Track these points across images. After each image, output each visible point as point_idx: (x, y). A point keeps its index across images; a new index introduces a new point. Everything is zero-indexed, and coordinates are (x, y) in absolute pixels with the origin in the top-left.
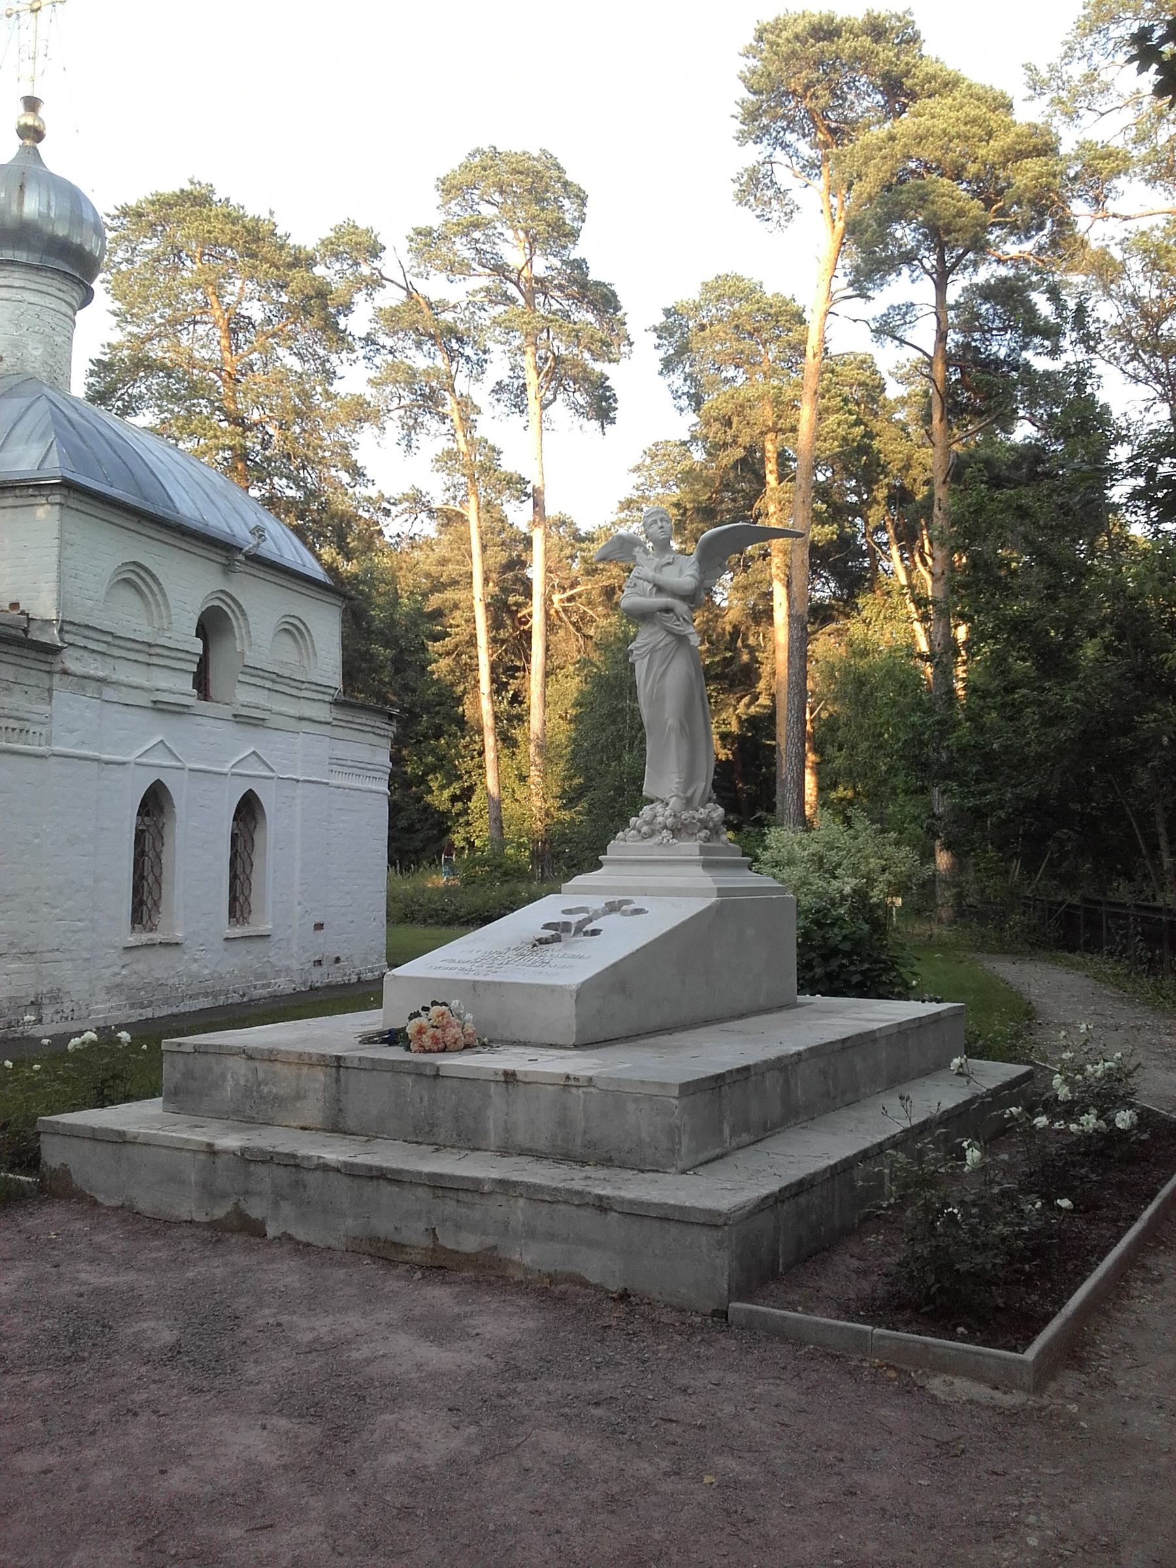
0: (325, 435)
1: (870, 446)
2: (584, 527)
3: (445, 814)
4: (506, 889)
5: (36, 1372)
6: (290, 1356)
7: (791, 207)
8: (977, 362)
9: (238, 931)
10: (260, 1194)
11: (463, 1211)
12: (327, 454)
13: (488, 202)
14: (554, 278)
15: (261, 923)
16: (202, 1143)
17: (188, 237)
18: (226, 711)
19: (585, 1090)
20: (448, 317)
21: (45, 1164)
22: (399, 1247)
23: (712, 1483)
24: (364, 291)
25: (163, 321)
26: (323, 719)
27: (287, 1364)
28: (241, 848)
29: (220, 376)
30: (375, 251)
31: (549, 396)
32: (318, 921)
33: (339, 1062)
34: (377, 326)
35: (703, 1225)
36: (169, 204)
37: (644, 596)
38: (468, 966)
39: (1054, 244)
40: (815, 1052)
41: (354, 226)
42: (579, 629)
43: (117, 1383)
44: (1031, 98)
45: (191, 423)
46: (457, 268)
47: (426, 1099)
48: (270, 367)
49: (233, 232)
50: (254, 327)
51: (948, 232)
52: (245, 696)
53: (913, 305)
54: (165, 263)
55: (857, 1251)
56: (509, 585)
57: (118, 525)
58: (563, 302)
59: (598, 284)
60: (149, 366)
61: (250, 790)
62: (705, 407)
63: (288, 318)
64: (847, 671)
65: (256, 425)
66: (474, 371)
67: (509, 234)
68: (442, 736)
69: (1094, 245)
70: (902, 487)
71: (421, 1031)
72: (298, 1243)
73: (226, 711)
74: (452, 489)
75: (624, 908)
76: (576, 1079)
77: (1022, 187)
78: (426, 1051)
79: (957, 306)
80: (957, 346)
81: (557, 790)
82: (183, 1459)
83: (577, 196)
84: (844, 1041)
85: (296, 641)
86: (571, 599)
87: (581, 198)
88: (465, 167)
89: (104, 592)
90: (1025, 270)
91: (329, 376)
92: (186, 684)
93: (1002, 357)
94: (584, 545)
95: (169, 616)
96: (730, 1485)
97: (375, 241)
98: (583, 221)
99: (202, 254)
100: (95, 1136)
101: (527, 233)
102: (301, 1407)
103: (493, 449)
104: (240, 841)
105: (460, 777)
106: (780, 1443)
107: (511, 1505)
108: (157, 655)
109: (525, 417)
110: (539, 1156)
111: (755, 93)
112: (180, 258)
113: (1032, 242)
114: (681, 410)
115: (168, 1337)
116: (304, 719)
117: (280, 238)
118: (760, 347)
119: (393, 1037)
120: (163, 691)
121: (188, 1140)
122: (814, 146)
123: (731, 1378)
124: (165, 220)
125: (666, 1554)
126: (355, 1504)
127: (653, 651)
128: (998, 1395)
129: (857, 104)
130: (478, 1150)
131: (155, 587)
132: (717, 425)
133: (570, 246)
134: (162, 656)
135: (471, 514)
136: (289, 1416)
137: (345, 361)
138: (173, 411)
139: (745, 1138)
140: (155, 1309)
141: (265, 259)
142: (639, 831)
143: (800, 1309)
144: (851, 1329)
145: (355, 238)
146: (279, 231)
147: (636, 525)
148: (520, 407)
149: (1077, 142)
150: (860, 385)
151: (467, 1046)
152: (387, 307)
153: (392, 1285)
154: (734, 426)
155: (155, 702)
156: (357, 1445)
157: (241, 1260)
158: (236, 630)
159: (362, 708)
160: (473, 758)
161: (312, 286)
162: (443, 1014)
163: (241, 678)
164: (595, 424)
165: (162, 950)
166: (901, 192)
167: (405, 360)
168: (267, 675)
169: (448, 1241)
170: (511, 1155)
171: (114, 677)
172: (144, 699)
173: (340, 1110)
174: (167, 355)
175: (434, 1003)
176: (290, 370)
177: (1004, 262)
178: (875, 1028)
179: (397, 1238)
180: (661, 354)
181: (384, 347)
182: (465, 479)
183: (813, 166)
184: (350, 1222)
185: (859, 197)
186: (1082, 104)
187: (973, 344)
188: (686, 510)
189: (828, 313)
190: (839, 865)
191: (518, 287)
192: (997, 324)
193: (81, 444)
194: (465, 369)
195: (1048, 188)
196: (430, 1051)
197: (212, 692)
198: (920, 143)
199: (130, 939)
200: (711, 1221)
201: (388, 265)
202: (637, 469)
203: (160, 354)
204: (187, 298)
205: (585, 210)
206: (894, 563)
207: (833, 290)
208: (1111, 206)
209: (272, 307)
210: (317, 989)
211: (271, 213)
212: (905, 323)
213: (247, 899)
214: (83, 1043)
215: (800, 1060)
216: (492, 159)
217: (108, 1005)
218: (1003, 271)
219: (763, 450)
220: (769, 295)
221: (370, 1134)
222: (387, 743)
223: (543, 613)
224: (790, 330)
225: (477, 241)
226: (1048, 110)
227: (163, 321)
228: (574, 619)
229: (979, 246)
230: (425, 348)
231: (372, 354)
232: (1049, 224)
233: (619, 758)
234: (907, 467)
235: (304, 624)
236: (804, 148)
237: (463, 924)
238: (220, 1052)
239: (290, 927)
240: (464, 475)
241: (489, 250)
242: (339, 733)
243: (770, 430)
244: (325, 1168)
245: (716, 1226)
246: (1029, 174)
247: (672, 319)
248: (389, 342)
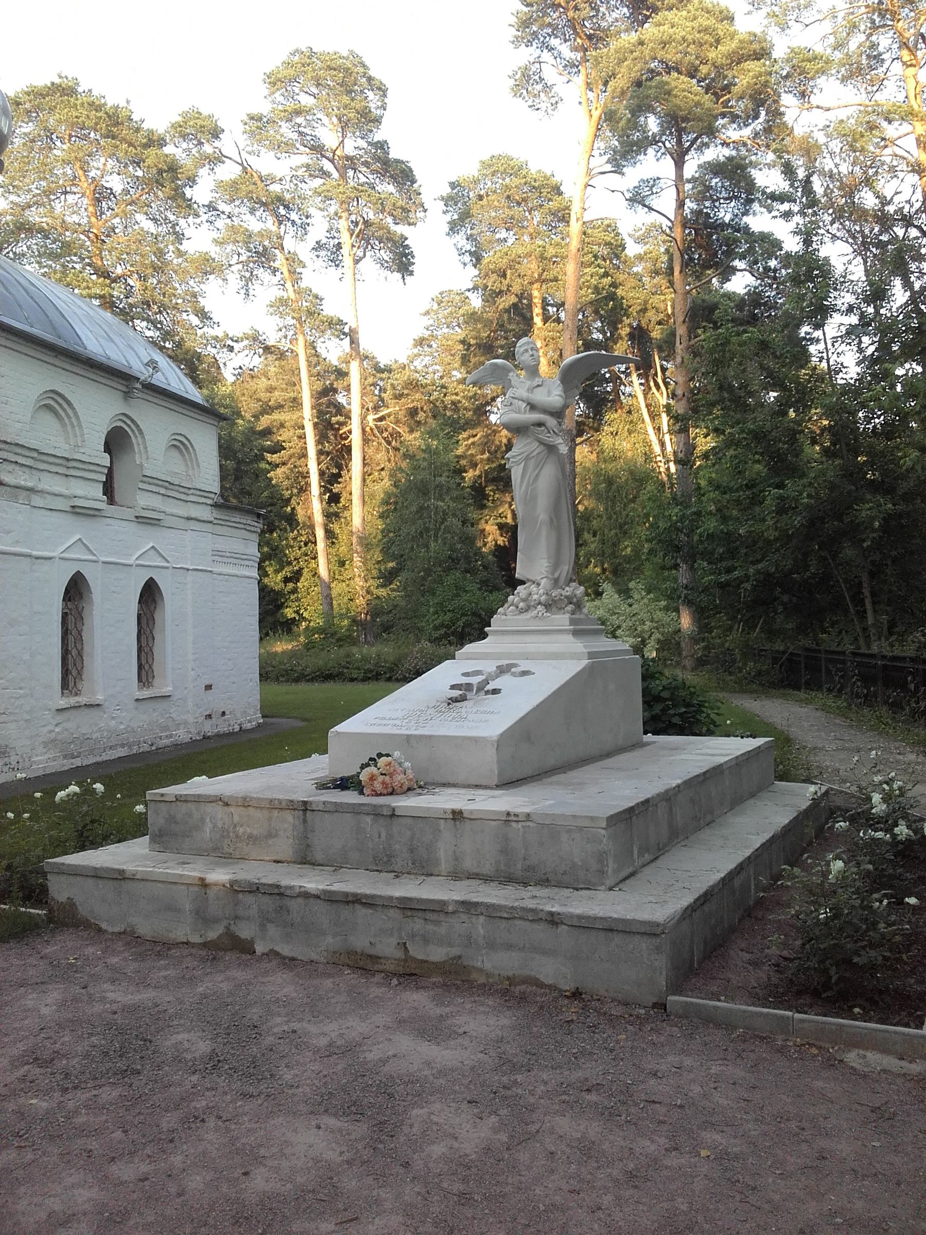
0: (177, 286)
1: (615, 293)
2: (383, 361)
3: (280, 594)
4: (342, 652)
5: (100, 1086)
6: (315, 1060)
7: (556, 99)
8: (707, 225)
9: (146, 693)
10: (248, 919)
11: (430, 927)
12: (180, 301)
13: (306, 93)
14: (362, 157)
15: (163, 686)
16: (194, 878)
17: (60, 121)
18: (130, 514)
19: (523, 824)
20: (275, 188)
21: (53, 899)
22: (375, 958)
23: (708, 1157)
24: (207, 166)
25: (38, 192)
26: (205, 519)
27: (316, 1067)
28: (144, 625)
29: (89, 237)
30: (216, 133)
31: (360, 253)
32: (208, 683)
33: (305, 807)
34: (217, 196)
35: (644, 934)
36: (41, 95)
37: (520, 412)
38: (398, 722)
39: (768, 130)
40: (689, 783)
41: (198, 112)
42: (389, 443)
43: (176, 1091)
44: (749, 13)
45: (67, 276)
46: (283, 147)
47: (383, 835)
48: (130, 229)
49: (97, 118)
50: (115, 197)
51: (685, 119)
52: (145, 501)
53: (659, 179)
54: (40, 143)
55: (743, 945)
56: (323, 408)
57: (32, 357)
58: (370, 176)
59: (398, 161)
60: (29, 229)
61: (151, 578)
62: (485, 261)
63: (143, 189)
64: (598, 474)
65: (119, 278)
66: (299, 233)
67: (325, 120)
68: (274, 530)
69: (799, 131)
70: (639, 327)
71: (372, 778)
72: (284, 958)
73: (130, 514)
74: (284, 330)
75: (513, 670)
76: (516, 815)
77: (745, 84)
78: (377, 795)
79: (693, 180)
80: (692, 212)
81: (375, 573)
82: (259, 1160)
83: (379, 89)
84: (705, 773)
85: (183, 455)
86: (381, 419)
87: (382, 91)
88: (287, 64)
89: (30, 415)
90: (743, 152)
91: (179, 237)
92: (97, 491)
93: (727, 221)
94: (384, 376)
95: (82, 435)
96: (722, 1157)
97: (216, 125)
98: (385, 109)
99: (70, 136)
100: (97, 874)
101: (340, 119)
102: (342, 1107)
103: (316, 297)
104: (144, 621)
105: (290, 563)
106: (749, 1117)
107: (550, 1186)
108: (74, 468)
109: (340, 269)
110: (486, 879)
111: (527, 5)
112: (51, 139)
113: (750, 128)
114: (465, 264)
115: (203, 1047)
116: (192, 519)
117: (136, 122)
118: (527, 213)
119: (344, 784)
120: (80, 497)
121: (181, 876)
122: (574, 49)
123: (688, 1062)
124: (38, 108)
125: (696, 1222)
126: (419, 1193)
127: (527, 459)
128: (903, 1063)
129: (607, 14)
130: (431, 875)
131: (70, 412)
132: (494, 277)
133: (375, 130)
134: (78, 469)
135: (300, 349)
136: (335, 1115)
137: (191, 225)
138: (51, 266)
139: (648, 857)
140: (182, 1022)
141: (123, 140)
142: (517, 607)
143: (723, 998)
144: (776, 1015)
145: (199, 122)
146: (135, 117)
147: (427, 358)
148: (336, 261)
149: (789, 47)
150: (606, 244)
151: (409, 789)
152: (228, 179)
153: (375, 991)
154: (508, 276)
155: (73, 507)
156: (402, 1139)
157: (239, 974)
158: (136, 446)
159: (236, 509)
160: (300, 548)
161: (165, 162)
162: (390, 764)
163: (141, 485)
164: (398, 276)
165: (86, 711)
166: (650, 87)
167: (242, 224)
168: (160, 483)
169: (417, 952)
170: (461, 879)
171: (40, 487)
172: (64, 505)
173: (308, 846)
174: (44, 220)
175: (380, 755)
176: (148, 233)
177: (728, 145)
178: (722, 762)
179: (372, 952)
180: (448, 217)
181: (223, 213)
182: (294, 321)
183: (573, 65)
184: (330, 939)
185: (614, 91)
186: (791, 17)
187: (705, 211)
188: (470, 345)
189: (587, 185)
190: (619, 627)
191: (333, 163)
192: (724, 194)
193: (5, 292)
194: (291, 230)
195: (766, 84)
196: (381, 795)
197: (117, 497)
198: (663, 48)
199: (61, 702)
200: (650, 931)
201: (226, 144)
202: (427, 313)
203: (38, 219)
204: (58, 173)
205: (386, 100)
206: (635, 386)
207: (591, 166)
208: (814, 100)
209: (129, 180)
210: (209, 737)
211: (128, 102)
212: (653, 193)
213: (150, 667)
214: (68, 795)
215: (679, 791)
216: (308, 58)
217: (46, 756)
218: (727, 152)
219: (531, 295)
220: (533, 171)
221: (336, 864)
222: (255, 538)
223: (360, 431)
224: (550, 200)
225: (299, 126)
226: (766, 22)
227: (38, 192)
228: (385, 435)
229: (712, 132)
230: (258, 214)
231: (213, 218)
232: (763, 113)
233: (427, 546)
234: (644, 310)
235: (189, 441)
236: (565, 50)
237: (308, 681)
238: (199, 800)
239: (186, 688)
240: (293, 318)
241: (309, 133)
242: (219, 530)
243: (537, 281)
244: (306, 895)
245: (654, 934)
246: (751, 74)
247: (454, 191)
248: (226, 208)
